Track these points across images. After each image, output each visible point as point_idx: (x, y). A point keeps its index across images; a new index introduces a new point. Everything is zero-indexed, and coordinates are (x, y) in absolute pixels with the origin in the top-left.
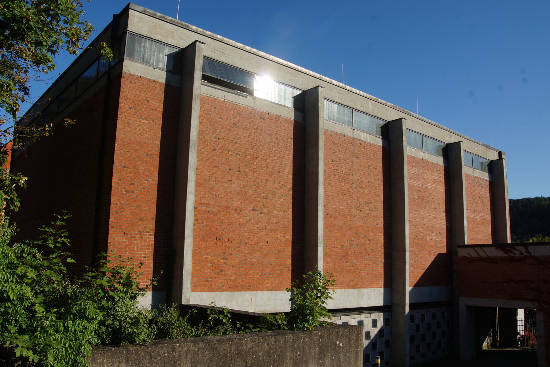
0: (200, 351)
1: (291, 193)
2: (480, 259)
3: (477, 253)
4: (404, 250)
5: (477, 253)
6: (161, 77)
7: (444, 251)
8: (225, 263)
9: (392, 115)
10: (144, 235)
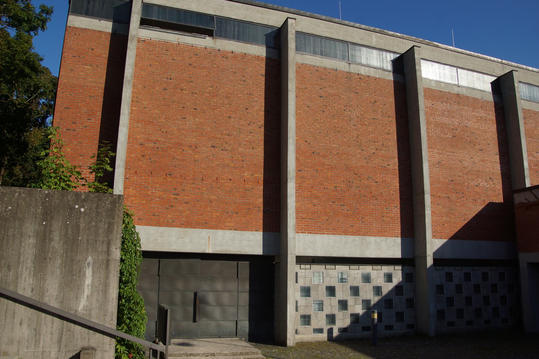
1: (262, 129)
5: (536, 197)
7: (499, 199)
8: (176, 199)
10: (84, 169)
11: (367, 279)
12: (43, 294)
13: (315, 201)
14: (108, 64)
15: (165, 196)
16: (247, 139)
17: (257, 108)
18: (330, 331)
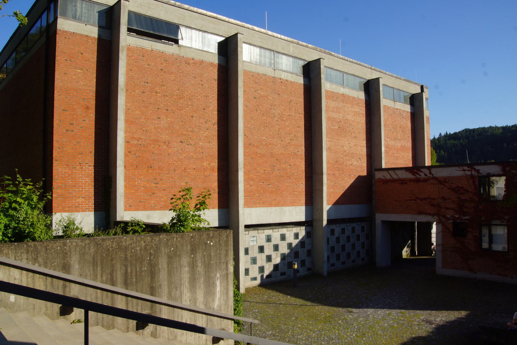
0: (87, 246)
1: (216, 126)
2: (393, 181)
3: (391, 175)
4: (322, 174)
5: (391, 175)
6: (93, 31)
7: (364, 173)
8: (156, 187)
9: (312, 56)
10: (84, 166)
11: (283, 237)
12: (196, 301)
13: (251, 183)
14: (97, 68)
15: (148, 185)
16: (205, 135)
17: (211, 108)
18: (262, 276)
